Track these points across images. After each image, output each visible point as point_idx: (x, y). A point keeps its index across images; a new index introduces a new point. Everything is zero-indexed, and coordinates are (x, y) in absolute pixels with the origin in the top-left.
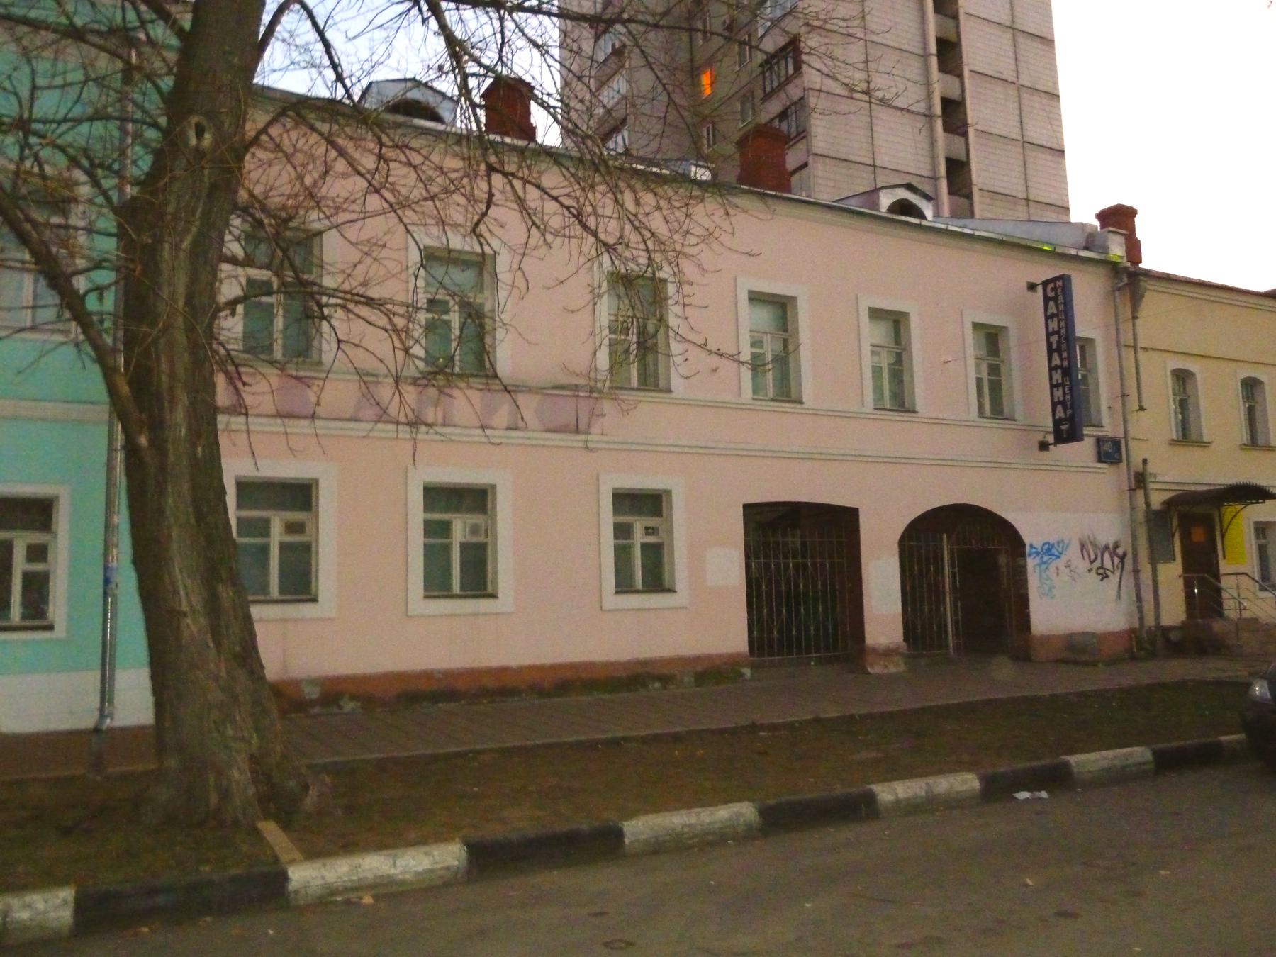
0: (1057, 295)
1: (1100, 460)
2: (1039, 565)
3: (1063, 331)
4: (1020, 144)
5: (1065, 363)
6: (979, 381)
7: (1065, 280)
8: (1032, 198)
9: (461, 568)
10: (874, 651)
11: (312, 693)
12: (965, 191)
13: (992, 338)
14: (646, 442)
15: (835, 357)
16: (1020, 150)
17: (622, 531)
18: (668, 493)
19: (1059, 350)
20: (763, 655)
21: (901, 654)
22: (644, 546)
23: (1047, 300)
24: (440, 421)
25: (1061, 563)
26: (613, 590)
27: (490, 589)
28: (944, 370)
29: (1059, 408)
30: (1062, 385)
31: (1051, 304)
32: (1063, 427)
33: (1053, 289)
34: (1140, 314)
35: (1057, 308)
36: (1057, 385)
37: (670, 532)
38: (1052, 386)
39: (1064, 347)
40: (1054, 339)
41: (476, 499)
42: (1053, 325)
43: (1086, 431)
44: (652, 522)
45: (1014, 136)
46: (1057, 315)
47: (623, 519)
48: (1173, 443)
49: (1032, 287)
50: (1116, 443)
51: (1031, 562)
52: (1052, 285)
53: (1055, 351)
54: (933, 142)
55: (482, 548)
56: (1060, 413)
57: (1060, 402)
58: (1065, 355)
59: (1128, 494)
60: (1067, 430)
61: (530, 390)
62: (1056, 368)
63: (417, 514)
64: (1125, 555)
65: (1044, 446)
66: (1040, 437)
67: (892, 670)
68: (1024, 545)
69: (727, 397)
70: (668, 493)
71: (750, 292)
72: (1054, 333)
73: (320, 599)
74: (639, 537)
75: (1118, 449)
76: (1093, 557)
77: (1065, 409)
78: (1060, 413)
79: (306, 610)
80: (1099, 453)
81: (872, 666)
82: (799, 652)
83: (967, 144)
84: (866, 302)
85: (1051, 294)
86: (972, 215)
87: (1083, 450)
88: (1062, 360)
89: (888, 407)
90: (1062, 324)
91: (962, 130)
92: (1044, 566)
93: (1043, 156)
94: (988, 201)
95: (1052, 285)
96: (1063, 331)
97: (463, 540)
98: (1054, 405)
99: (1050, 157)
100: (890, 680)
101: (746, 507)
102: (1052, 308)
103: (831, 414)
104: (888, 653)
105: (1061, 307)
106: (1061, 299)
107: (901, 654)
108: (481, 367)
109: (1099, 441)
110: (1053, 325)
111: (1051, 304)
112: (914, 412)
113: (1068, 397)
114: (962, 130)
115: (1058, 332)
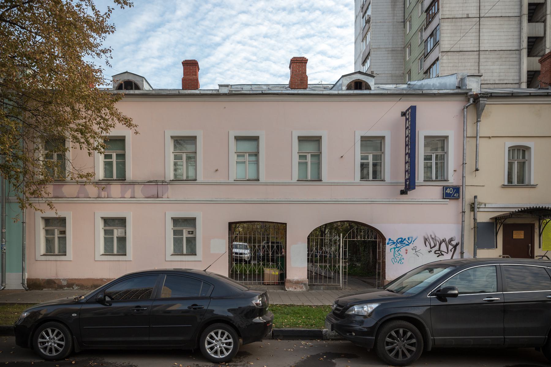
2: (394, 248)
9: (117, 245)
10: (290, 281)
11: (65, 283)
14: (181, 201)
20: (322, 262)
21: (305, 284)
24: (106, 196)
25: (409, 248)
34: (482, 119)
40: (407, 139)
48: (504, 186)
51: (388, 247)
59: (461, 215)
61: (138, 183)
64: (457, 244)
67: (298, 290)
68: (384, 239)
69: (222, 180)
71: (299, 137)
74: (185, 235)
76: (433, 245)
79: (63, 258)
81: (288, 288)
82: (259, 280)
84: (233, 134)
89: (309, 178)
92: (397, 249)
100: (296, 294)
103: (273, 184)
104: (297, 283)
107: (305, 284)
108: (122, 178)
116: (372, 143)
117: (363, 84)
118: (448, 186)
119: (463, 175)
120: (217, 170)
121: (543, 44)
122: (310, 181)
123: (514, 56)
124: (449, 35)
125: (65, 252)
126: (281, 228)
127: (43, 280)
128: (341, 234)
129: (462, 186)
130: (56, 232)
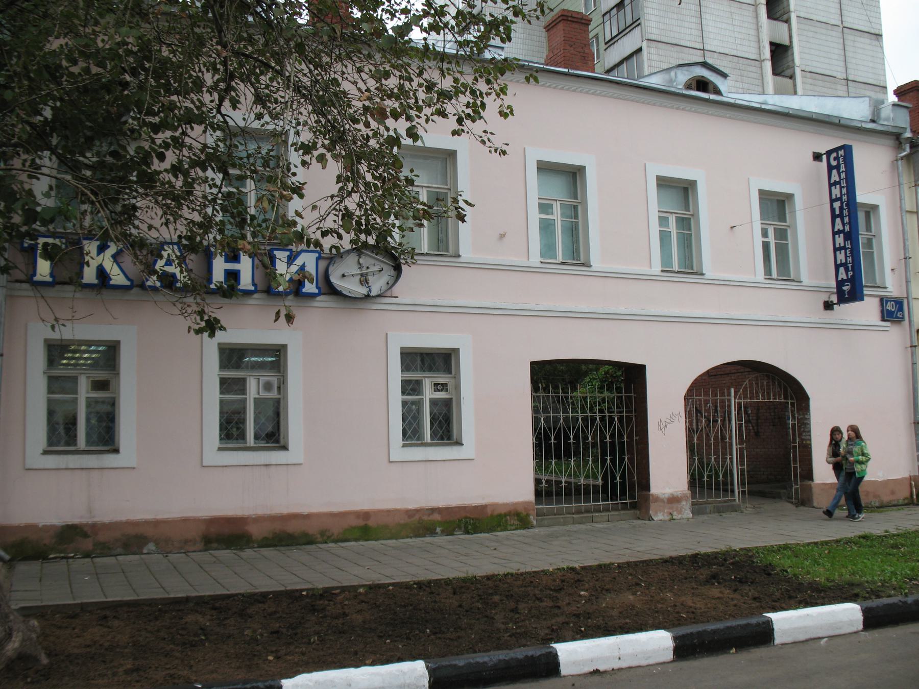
0: (840, 164)
1: (883, 320)
3: (845, 198)
4: (840, 29)
5: (847, 228)
6: (766, 246)
7: (847, 149)
8: (850, 78)
9: (255, 424)
10: (657, 499)
12: (788, 72)
13: (776, 205)
15: (624, 223)
16: (840, 35)
17: (410, 387)
18: (456, 351)
19: (841, 216)
22: (433, 402)
23: (830, 168)
26: (401, 443)
27: (282, 443)
28: (730, 232)
29: (842, 270)
30: (844, 248)
31: (834, 172)
32: (845, 288)
33: (836, 159)
35: (840, 176)
36: (840, 249)
37: (458, 387)
38: (836, 250)
39: (845, 212)
40: (837, 205)
41: (442, 361)
42: (836, 191)
43: (866, 291)
44: (442, 378)
45: (833, 22)
46: (839, 183)
47: (413, 376)
49: (817, 157)
50: (899, 303)
52: (834, 155)
53: (838, 216)
54: (758, 28)
55: (448, 403)
56: (842, 275)
57: (842, 265)
58: (846, 220)
60: (849, 290)
62: (839, 232)
63: (396, 376)
65: (828, 306)
66: (825, 297)
69: (645, 270)
70: (456, 351)
72: (837, 200)
73: (121, 450)
74: (428, 394)
75: (901, 309)
77: (847, 271)
78: (842, 275)
79: (109, 460)
80: (882, 312)
81: (656, 513)
83: (790, 30)
85: (834, 163)
86: (795, 93)
87: (866, 311)
88: (844, 225)
89: (676, 268)
90: (844, 191)
91: (785, 17)
93: (862, 40)
94: (810, 81)
95: (834, 155)
96: (845, 198)
97: (257, 396)
98: (837, 267)
99: (868, 41)
101: (532, 363)
102: (835, 177)
104: (673, 500)
105: (843, 176)
106: (843, 168)
109: (883, 301)
110: (836, 191)
111: (834, 172)
112: (702, 274)
113: (850, 260)
114: (785, 17)
115: (840, 199)
116: (776, 205)
117: (711, 87)
118: (886, 297)
119: (906, 278)
120: (502, 236)
121: (790, 58)
122: (678, 272)
123: (754, 69)
124: (656, 12)
125: (403, 406)
126: (631, 377)
127: (46, 528)
128: (732, 390)
129: (907, 298)
130: (84, 385)
